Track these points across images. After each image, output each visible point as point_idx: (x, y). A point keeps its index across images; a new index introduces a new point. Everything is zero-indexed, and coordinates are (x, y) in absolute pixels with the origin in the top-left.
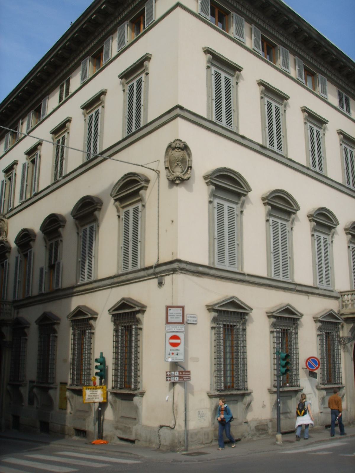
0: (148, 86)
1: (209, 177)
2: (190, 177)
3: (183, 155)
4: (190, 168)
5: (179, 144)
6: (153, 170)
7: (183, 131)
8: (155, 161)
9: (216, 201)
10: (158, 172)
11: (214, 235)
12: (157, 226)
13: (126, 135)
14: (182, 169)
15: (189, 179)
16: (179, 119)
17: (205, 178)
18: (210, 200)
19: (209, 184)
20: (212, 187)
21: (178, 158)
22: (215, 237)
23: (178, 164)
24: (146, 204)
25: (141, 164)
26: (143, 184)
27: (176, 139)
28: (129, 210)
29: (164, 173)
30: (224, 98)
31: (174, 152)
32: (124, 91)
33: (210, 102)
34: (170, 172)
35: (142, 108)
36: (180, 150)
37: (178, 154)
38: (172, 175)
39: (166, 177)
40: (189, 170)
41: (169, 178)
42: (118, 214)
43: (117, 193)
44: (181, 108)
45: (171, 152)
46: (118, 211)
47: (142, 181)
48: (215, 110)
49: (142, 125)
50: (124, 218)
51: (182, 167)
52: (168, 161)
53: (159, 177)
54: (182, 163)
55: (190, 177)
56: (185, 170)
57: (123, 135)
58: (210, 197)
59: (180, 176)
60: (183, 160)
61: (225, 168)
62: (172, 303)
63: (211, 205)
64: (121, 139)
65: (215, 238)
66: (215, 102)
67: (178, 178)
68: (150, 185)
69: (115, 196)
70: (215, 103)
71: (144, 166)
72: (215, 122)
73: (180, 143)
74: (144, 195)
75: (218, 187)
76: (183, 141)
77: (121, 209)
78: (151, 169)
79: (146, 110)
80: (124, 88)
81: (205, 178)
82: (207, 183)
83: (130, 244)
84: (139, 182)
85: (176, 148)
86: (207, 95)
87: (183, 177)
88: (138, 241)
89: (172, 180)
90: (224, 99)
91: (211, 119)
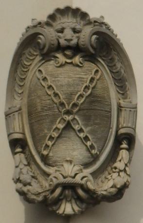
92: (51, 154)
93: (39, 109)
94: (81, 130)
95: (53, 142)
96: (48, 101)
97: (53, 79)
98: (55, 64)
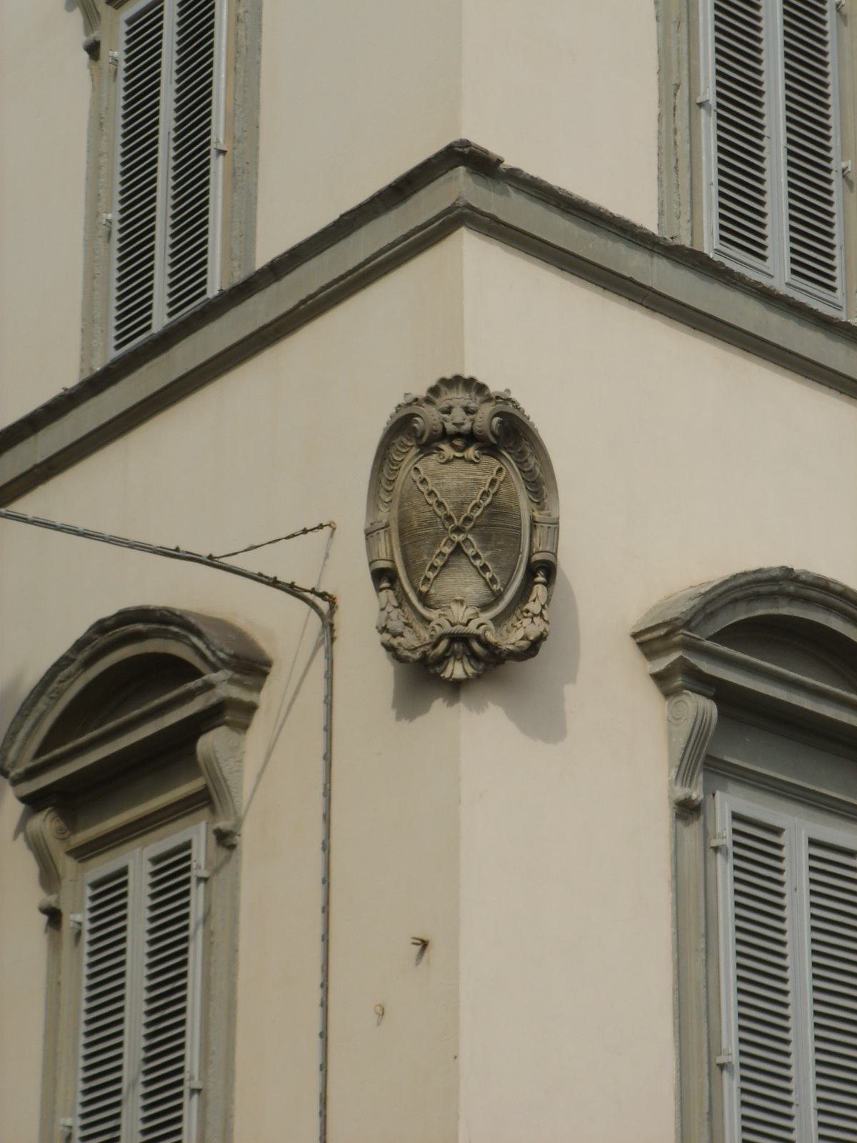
0: (259, 16)
1: (677, 638)
2: (542, 638)
3: (493, 482)
4: (540, 578)
5: (468, 411)
6: (292, 589)
7: (497, 318)
8: (305, 531)
9: (728, 802)
10: (324, 605)
11: (713, 1045)
12: (317, 978)
13: (108, 353)
14: (490, 583)
15: (534, 647)
16: (466, 241)
17: (649, 641)
18: (681, 793)
19: (679, 681)
20: (698, 706)
21: (460, 506)
22: (721, 1059)
23: (458, 550)
24: (239, 822)
25: (204, 553)
26: (225, 687)
27: (449, 375)
28: (124, 872)
29: (362, 608)
30: (782, 92)
31: (431, 463)
32: (93, 50)
33: (682, 123)
34: (402, 600)
35: (218, 167)
36: (471, 452)
37: (457, 478)
38: (418, 626)
39: (378, 638)
40: (539, 591)
41: (395, 642)
42: (51, 900)
43: (44, 748)
44: (482, 164)
45: (409, 462)
46: (49, 877)
47: (215, 669)
48: (715, 177)
49: (215, 285)
50: (88, 926)
51: (485, 568)
52: (394, 527)
53: (332, 640)
54: (486, 540)
55: (542, 638)
56: (506, 587)
57: (87, 351)
58: (685, 773)
59: (472, 628)
60: (494, 523)
61: (788, 575)
62: (319, 582)
63: (692, 832)
64: (71, 379)
65: (722, 1067)
66: (713, 121)
67: (460, 642)
68: (270, 697)
69: (30, 774)
70: (713, 132)
71: (229, 561)
72: (717, 258)
73: (472, 405)
74: (227, 768)
75: (738, 708)
76: (495, 388)
77: (68, 865)
78: (274, 583)
79: (244, 179)
80: (95, 35)
81: (649, 641)
82: (659, 678)
83: (125, 1110)
84: (197, 674)
85: (445, 436)
86: (663, 72)
87: (491, 637)
88: (185, 1088)
89: (417, 656)
90: (782, 103)
91: (685, 241)
92: (432, 591)
93: (415, 524)
94: (477, 556)
95: (436, 573)
96: (429, 514)
97: (436, 481)
98: (439, 460)
